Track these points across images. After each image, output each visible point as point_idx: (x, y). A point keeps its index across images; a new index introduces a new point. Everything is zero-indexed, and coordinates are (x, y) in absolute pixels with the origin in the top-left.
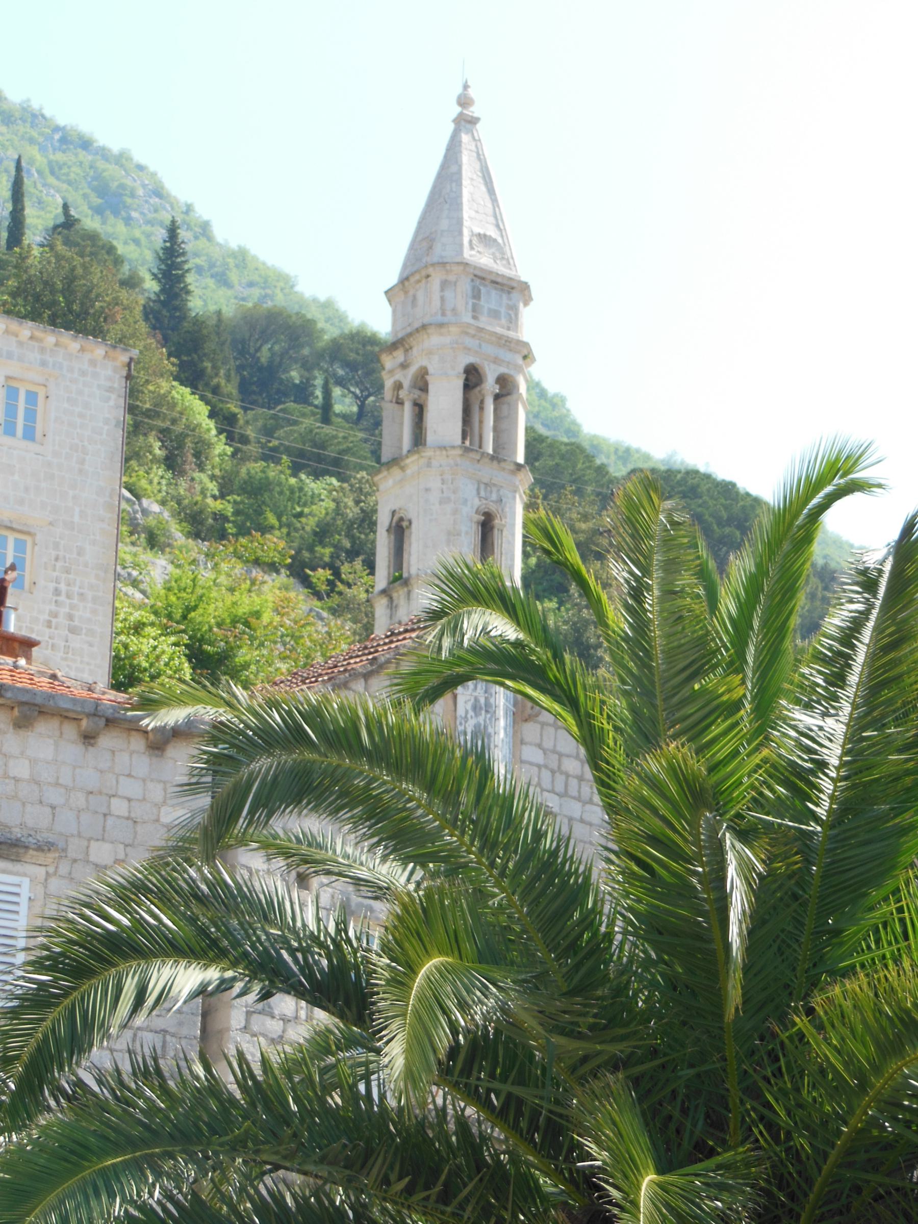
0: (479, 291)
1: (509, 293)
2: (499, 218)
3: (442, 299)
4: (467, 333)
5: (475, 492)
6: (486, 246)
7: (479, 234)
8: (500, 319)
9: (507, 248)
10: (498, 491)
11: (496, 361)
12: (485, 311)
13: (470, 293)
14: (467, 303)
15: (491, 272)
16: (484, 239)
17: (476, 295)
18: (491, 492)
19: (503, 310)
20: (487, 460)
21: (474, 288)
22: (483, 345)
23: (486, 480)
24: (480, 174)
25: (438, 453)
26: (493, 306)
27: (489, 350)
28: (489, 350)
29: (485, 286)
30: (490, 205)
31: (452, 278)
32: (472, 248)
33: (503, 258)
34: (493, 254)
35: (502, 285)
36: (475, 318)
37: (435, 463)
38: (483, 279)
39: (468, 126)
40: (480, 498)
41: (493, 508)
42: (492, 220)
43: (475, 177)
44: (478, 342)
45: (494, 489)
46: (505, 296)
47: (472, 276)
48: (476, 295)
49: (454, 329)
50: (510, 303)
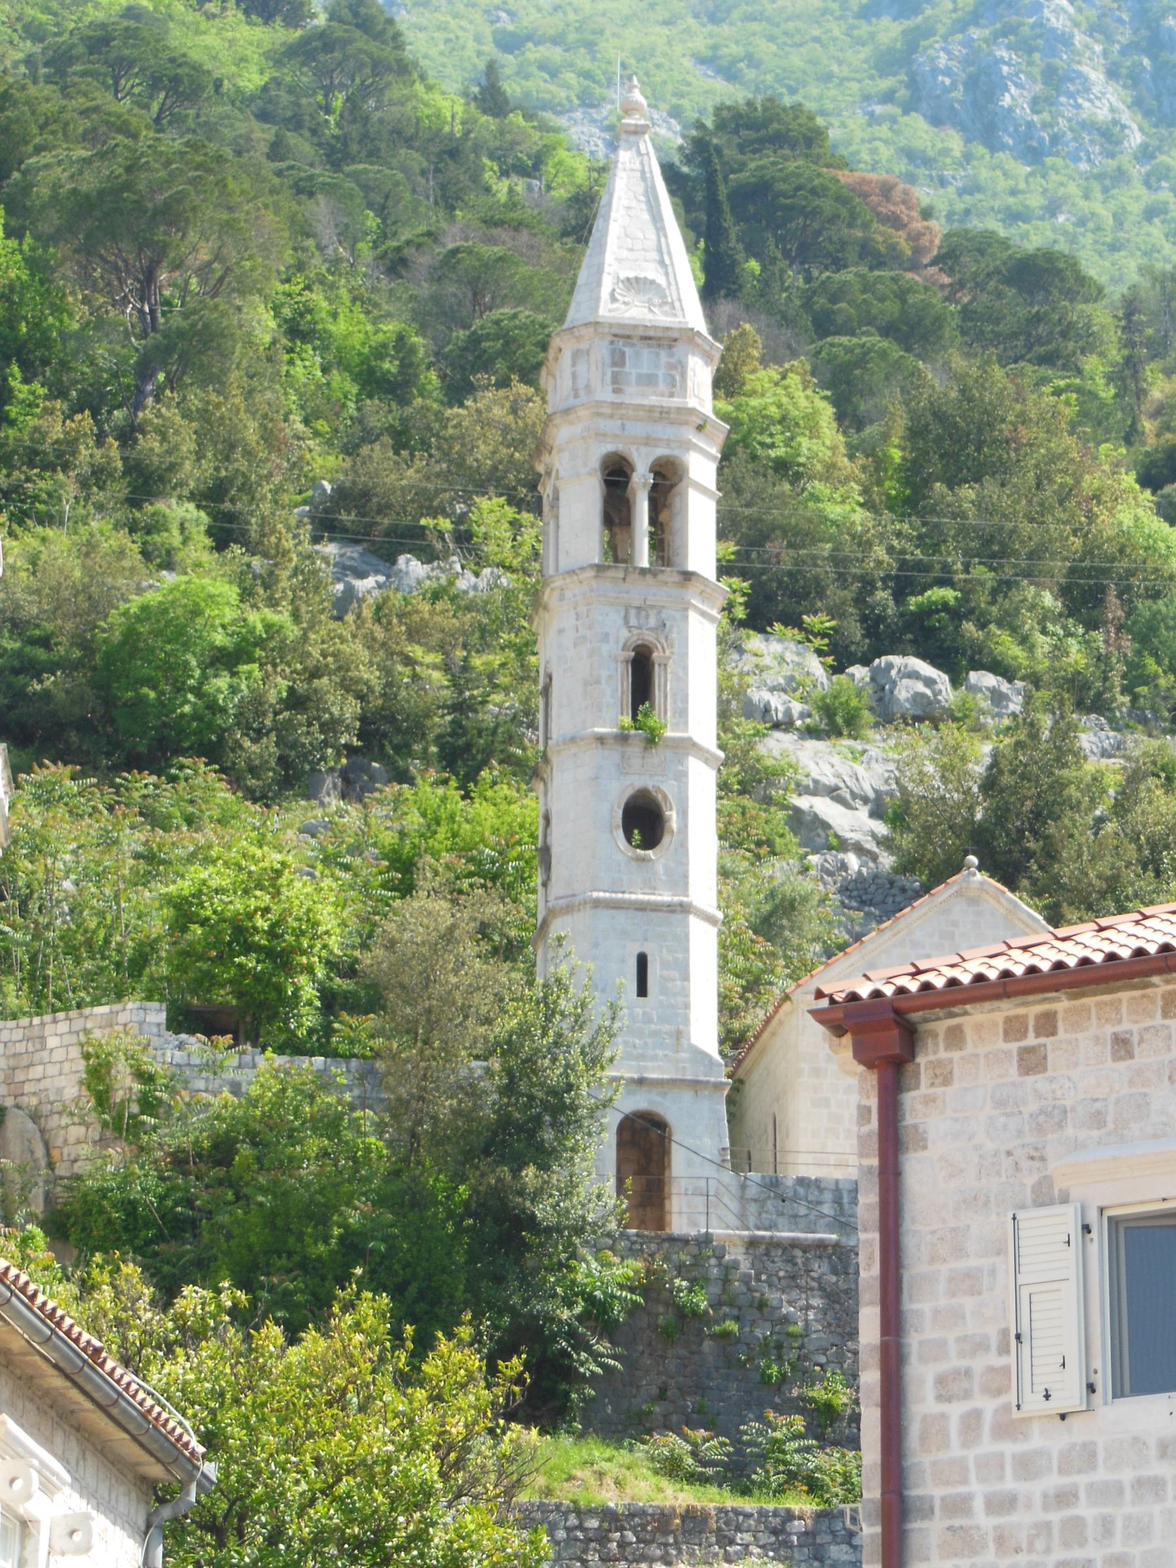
0: (623, 354)
1: (670, 347)
2: (664, 250)
3: (574, 376)
4: (599, 415)
5: (620, 622)
6: (638, 292)
7: (628, 279)
8: (656, 384)
9: (673, 288)
10: (659, 613)
11: (648, 441)
12: (633, 378)
13: (608, 361)
14: (604, 374)
15: (635, 327)
16: (635, 284)
17: (618, 360)
18: (647, 617)
19: (661, 373)
20: (636, 576)
21: (613, 352)
22: (628, 424)
23: (637, 603)
24: (642, 198)
25: (568, 580)
26: (645, 370)
27: (638, 429)
28: (638, 429)
29: (633, 345)
30: (653, 237)
31: (584, 346)
32: (614, 299)
33: (664, 303)
34: (650, 301)
35: (659, 339)
36: (616, 391)
37: (568, 594)
38: (629, 337)
39: (632, 138)
40: (629, 628)
41: (650, 637)
42: (654, 255)
43: (634, 204)
44: (619, 422)
45: (652, 613)
46: (663, 354)
47: (610, 338)
48: (618, 360)
49: (582, 413)
50: (672, 360)
